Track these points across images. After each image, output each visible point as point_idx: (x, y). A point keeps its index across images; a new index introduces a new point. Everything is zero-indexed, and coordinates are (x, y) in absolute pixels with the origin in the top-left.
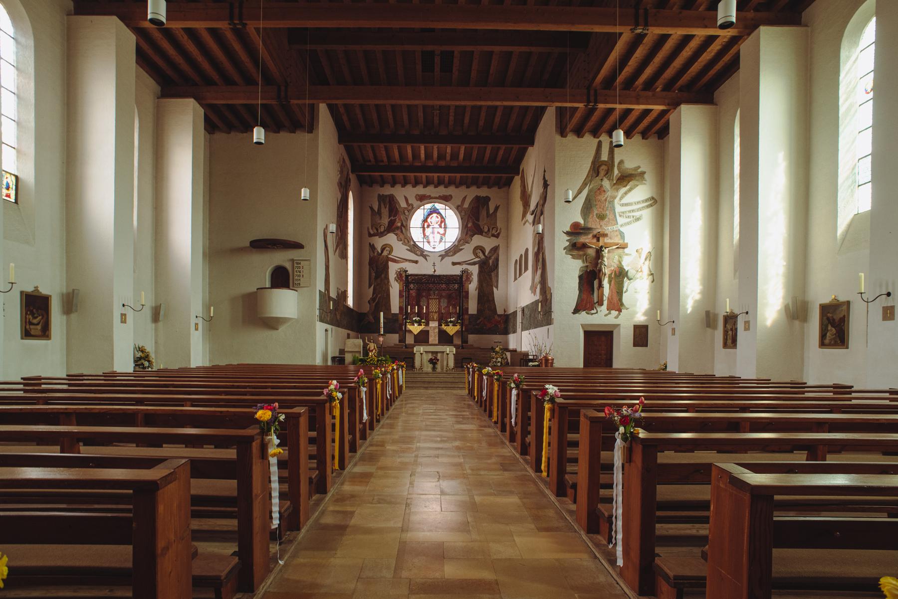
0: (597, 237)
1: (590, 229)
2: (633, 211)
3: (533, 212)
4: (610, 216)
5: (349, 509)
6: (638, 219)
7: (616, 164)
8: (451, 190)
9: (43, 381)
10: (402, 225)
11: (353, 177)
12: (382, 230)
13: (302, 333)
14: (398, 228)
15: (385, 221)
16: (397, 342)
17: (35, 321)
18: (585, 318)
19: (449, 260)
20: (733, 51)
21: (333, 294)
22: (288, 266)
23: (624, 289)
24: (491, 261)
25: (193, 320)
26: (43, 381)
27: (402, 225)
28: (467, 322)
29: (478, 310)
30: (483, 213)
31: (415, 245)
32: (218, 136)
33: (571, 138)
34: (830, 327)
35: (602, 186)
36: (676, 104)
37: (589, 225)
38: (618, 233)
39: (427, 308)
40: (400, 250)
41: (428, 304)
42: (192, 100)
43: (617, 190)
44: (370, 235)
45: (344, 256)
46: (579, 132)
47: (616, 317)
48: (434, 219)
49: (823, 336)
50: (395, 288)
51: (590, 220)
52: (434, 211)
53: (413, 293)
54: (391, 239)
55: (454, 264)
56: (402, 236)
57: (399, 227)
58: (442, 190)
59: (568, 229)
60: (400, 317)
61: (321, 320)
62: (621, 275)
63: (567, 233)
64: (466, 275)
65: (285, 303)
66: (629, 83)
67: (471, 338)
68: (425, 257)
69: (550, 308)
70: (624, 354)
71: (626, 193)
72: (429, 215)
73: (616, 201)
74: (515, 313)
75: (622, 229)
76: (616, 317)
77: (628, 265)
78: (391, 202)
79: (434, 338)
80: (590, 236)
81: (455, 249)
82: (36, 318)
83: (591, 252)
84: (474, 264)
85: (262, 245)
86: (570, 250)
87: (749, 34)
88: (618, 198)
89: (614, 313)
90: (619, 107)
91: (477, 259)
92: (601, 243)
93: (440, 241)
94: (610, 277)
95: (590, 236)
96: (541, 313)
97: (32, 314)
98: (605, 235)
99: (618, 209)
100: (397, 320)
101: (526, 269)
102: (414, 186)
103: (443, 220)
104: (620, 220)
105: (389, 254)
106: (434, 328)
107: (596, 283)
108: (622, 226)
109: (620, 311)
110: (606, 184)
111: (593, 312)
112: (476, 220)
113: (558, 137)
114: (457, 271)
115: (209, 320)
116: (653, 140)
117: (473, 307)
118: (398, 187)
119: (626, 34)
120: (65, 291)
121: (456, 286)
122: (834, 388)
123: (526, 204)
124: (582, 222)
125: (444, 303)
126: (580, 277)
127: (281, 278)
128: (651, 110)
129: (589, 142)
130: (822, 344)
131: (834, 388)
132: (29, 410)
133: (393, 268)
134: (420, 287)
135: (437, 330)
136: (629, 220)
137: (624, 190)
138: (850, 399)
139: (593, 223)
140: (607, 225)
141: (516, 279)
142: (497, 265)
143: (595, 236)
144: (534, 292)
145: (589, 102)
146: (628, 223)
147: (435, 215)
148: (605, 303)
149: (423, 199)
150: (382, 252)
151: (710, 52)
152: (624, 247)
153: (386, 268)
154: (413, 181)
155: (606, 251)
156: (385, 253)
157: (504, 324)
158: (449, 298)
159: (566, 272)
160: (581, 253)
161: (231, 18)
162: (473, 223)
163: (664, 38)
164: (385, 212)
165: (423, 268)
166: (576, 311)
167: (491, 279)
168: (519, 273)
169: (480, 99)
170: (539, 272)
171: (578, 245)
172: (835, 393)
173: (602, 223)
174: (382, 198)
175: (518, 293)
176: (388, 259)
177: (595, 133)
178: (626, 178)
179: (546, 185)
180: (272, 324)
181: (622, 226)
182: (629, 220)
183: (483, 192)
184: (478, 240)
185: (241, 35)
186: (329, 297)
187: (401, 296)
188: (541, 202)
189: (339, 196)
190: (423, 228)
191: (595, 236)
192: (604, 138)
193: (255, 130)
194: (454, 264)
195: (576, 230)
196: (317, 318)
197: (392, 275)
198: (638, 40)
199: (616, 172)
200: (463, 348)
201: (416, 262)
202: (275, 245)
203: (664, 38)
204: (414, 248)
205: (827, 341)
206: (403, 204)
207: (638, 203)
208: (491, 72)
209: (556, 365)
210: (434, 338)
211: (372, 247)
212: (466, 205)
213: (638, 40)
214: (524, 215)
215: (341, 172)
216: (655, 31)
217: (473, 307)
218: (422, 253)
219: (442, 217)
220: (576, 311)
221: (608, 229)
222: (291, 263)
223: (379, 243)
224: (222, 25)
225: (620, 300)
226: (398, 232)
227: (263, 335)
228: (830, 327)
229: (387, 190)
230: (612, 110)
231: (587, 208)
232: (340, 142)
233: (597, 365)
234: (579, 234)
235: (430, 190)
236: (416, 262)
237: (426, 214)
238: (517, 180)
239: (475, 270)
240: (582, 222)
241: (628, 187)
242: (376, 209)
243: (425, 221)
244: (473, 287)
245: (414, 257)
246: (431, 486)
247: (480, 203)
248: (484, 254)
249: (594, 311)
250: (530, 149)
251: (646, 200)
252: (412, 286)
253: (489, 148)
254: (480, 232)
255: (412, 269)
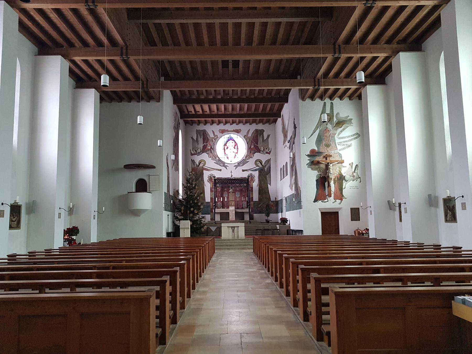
0: (326, 157)
1: (321, 153)
2: (346, 141)
3: (289, 141)
4: (333, 145)
5: (202, 303)
6: (349, 146)
7: (335, 115)
8: (241, 126)
9: (37, 254)
10: (211, 148)
11: (181, 121)
12: (199, 151)
13: (153, 219)
14: (208, 150)
15: (201, 146)
16: (210, 220)
17: (14, 220)
18: (321, 205)
19: (240, 168)
20: (388, 63)
21: (171, 194)
22: (146, 179)
23: (344, 187)
24: (266, 168)
25: (93, 214)
26: (37, 254)
27: (211, 148)
28: (252, 206)
29: (259, 199)
30: (260, 139)
31: (220, 160)
32: (104, 103)
33: (308, 101)
34: (448, 211)
35: (327, 128)
36: (396, 52)
37: (321, 151)
38: (338, 154)
39: (228, 198)
40: (210, 163)
41: (228, 196)
42: (93, 90)
43: (336, 130)
44: (192, 154)
45: (177, 169)
46: (312, 98)
47: (340, 204)
48: (231, 144)
49: (446, 216)
50: (208, 187)
51: (321, 147)
52: (230, 139)
53: (219, 189)
54: (204, 156)
55: (243, 171)
56: (211, 155)
57: (207, 146)
58: (235, 127)
59: (309, 153)
60: (211, 204)
61: (166, 210)
62: (341, 178)
63: (308, 156)
64: (251, 176)
65: (145, 201)
66: (337, 75)
67: (255, 215)
68: (226, 167)
69: (301, 199)
70: (346, 227)
71: (341, 131)
72: (227, 141)
73: (336, 136)
74: (282, 200)
75: (340, 152)
76: (340, 204)
77: (345, 173)
78: (204, 135)
79: (232, 217)
80: (322, 157)
81: (243, 162)
82: (14, 218)
83: (323, 166)
84: (256, 170)
85: (129, 167)
86: (310, 165)
87: (395, 55)
88: (337, 134)
89: (338, 201)
90: (333, 88)
91: (257, 168)
92: (328, 161)
93: (235, 157)
94: (334, 180)
95: (322, 157)
96: (296, 201)
97: (13, 216)
98: (331, 156)
99: (337, 141)
100: (209, 206)
101: (287, 174)
102: (218, 125)
103: (236, 144)
104: (339, 147)
105: (204, 166)
106: (233, 210)
107: (326, 184)
108: (340, 150)
109: (342, 200)
110: (329, 126)
111: (325, 201)
112: (256, 144)
113: (301, 101)
114: (245, 175)
115: (100, 212)
116: (356, 100)
117: (256, 197)
118: (208, 125)
119: (330, 58)
120: (28, 201)
121: (245, 185)
122: (434, 246)
123: (285, 136)
124: (316, 149)
125: (238, 195)
126: (317, 181)
127: (142, 186)
128: (406, 7)
129: (318, 103)
130: (446, 221)
131: (434, 246)
132: (20, 270)
133: (206, 175)
134: (222, 185)
135: (234, 212)
136: (344, 147)
137: (340, 130)
138: (440, 252)
139: (323, 149)
140: (331, 150)
141: (281, 180)
142: (270, 170)
143: (324, 157)
144: (292, 189)
145: (315, 86)
146: (344, 149)
147: (231, 141)
148: (333, 195)
149: (223, 132)
150: (199, 165)
151: (378, 61)
152: (342, 162)
153: (202, 174)
154: (217, 122)
155: (331, 165)
156: (201, 165)
157: (275, 206)
158: (241, 191)
159: (309, 178)
160: (317, 167)
161: (122, 55)
162: (255, 145)
163: (350, 59)
164: (201, 140)
165: (225, 174)
166: (315, 201)
167: (266, 179)
168: (283, 177)
169: (255, 86)
170: (294, 177)
171: (315, 162)
172: (434, 249)
173: (328, 149)
174: (198, 132)
175: (282, 188)
176: (203, 169)
177: (321, 98)
178: (340, 123)
179: (295, 127)
180: (136, 213)
181: (340, 150)
182: (344, 147)
183: (260, 127)
184: (257, 156)
185: (93, 12)
186: (169, 195)
187: (211, 191)
188: (293, 137)
189: (174, 134)
190: (224, 149)
191: (324, 157)
192: (327, 101)
193: (138, 117)
194: (243, 171)
195: (313, 154)
196: (163, 209)
197: (206, 178)
198: (336, 60)
199: (335, 119)
200: (250, 223)
201: (220, 170)
202: (139, 167)
203: (350, 59)
204: (219, 162)
205: (448, 219)
206: (212, 135)
207: (349, 136)
208: (261, 67)
209: (305, 234)
210: (232, 217)
211: (193, 162)
212: (250, 135)
213: (336, 60)
214: (284, 143)
215: (175, 120)
216: (344, 56)
217: (256, 197)
218: (224, 165)
219: (235, 143)
220: (315, 201)
221: (332, 152)
222: (148, 177)
223: (197, 159)
224: (117, 59)
225: (342, 193)
226: (209, 152)
227: (131, 220)
228: (448, 211)
229: (202, 127)
230: (328, 89)
231: (319, 141)
232: (174, 103)
233: (330, 233)
234: (315, 156)
235: (228, 127)
236: (220, 170)
237: (226, 141)
238: (279, 120)
239: (256, 174)
240: (316, 149)
241: (342, 128)
242: (195, 139)
243: (225, 145)
244: (255, 185)
245: (219, 167)
246: (234, 300)
247: (259, 133)
248: (262, 164)
249: (327, 200)
250: (286, 105)
251: (354, 135)
252: (218, 185)
253: (262, 105)
254: (259, 151)
255: (218, 175)
